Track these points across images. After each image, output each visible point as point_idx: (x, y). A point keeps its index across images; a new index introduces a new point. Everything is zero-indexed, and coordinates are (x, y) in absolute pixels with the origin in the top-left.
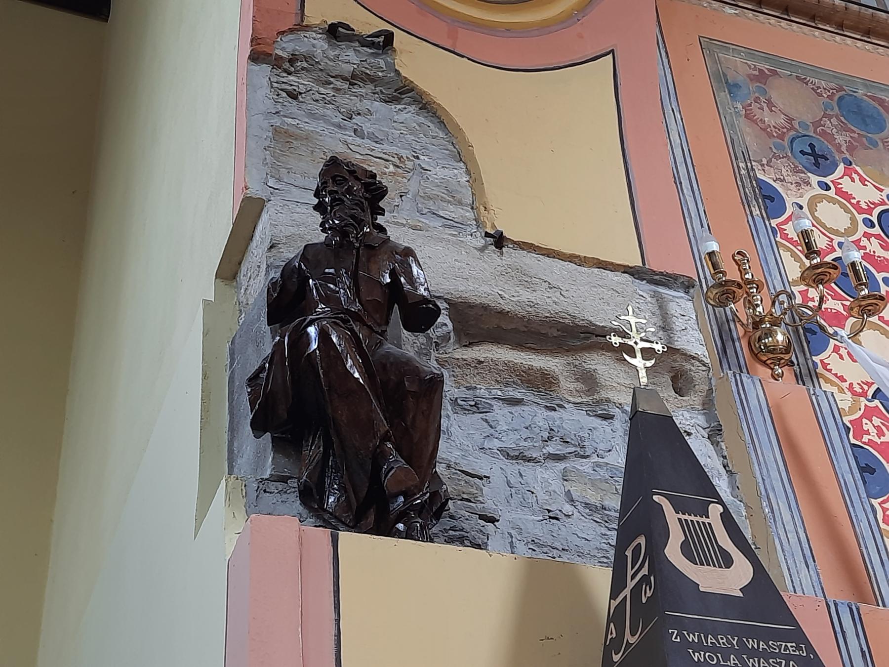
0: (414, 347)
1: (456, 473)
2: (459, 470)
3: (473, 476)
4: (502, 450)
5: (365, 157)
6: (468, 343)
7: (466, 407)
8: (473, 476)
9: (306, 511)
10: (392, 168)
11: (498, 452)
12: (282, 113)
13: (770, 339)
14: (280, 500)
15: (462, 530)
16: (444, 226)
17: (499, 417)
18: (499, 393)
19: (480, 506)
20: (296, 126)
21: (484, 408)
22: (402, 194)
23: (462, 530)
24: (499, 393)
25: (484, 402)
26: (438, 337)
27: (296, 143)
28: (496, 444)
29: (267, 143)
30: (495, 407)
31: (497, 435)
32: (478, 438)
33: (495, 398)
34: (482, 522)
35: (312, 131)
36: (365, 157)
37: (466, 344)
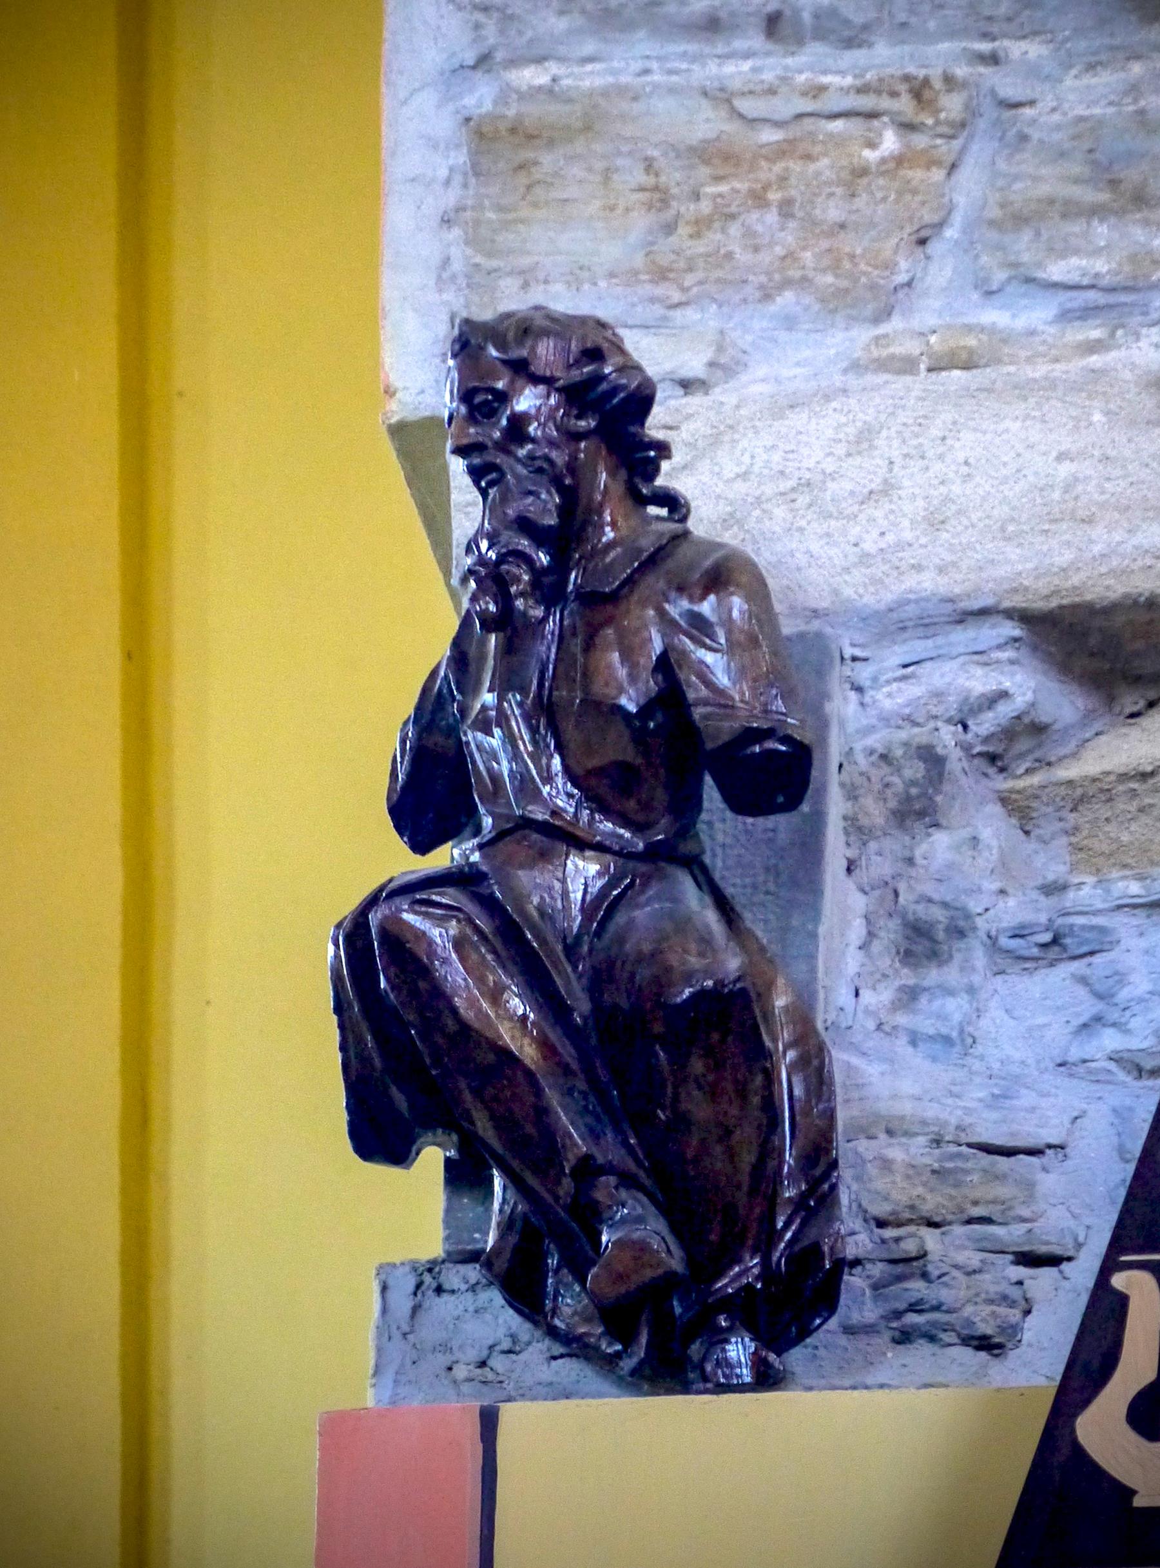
0: (885, 800)
1: (959, 1155)
2: (969, 1145)
3: (1009, 1152)
4: (1122, 1058)
5: (794, 131)
6: (1142, 704)
7: (1026, 953)
8: (1009, 1152)
9: (528, 1326)
10: (890, 142)
11: (1112, 1066)
12: (499, 56)
13: (1050, 1113)
14: (471, 1309)
15: (937, 1308)
16: (1065, 316)
17: (1132, 960)
18: (1135, 888)
19: (1019, 1229)
20: (550, 92)
21: (1081, 944)
22: (924, 234)
23: (937, 1308)
24: (1135, 888)
25: (1083, 928)
26: (986, 740)
27: (548, 161)
28: (1110, 1040)
29: (451, 197)
30: (1122, 933)
31: (1115, 1015)
32: (1057, 1034)
33: (1120, 907)
34: (1022, 1272)
35: (605, 93)
36: (794, 131)
37: (1135, 709)
